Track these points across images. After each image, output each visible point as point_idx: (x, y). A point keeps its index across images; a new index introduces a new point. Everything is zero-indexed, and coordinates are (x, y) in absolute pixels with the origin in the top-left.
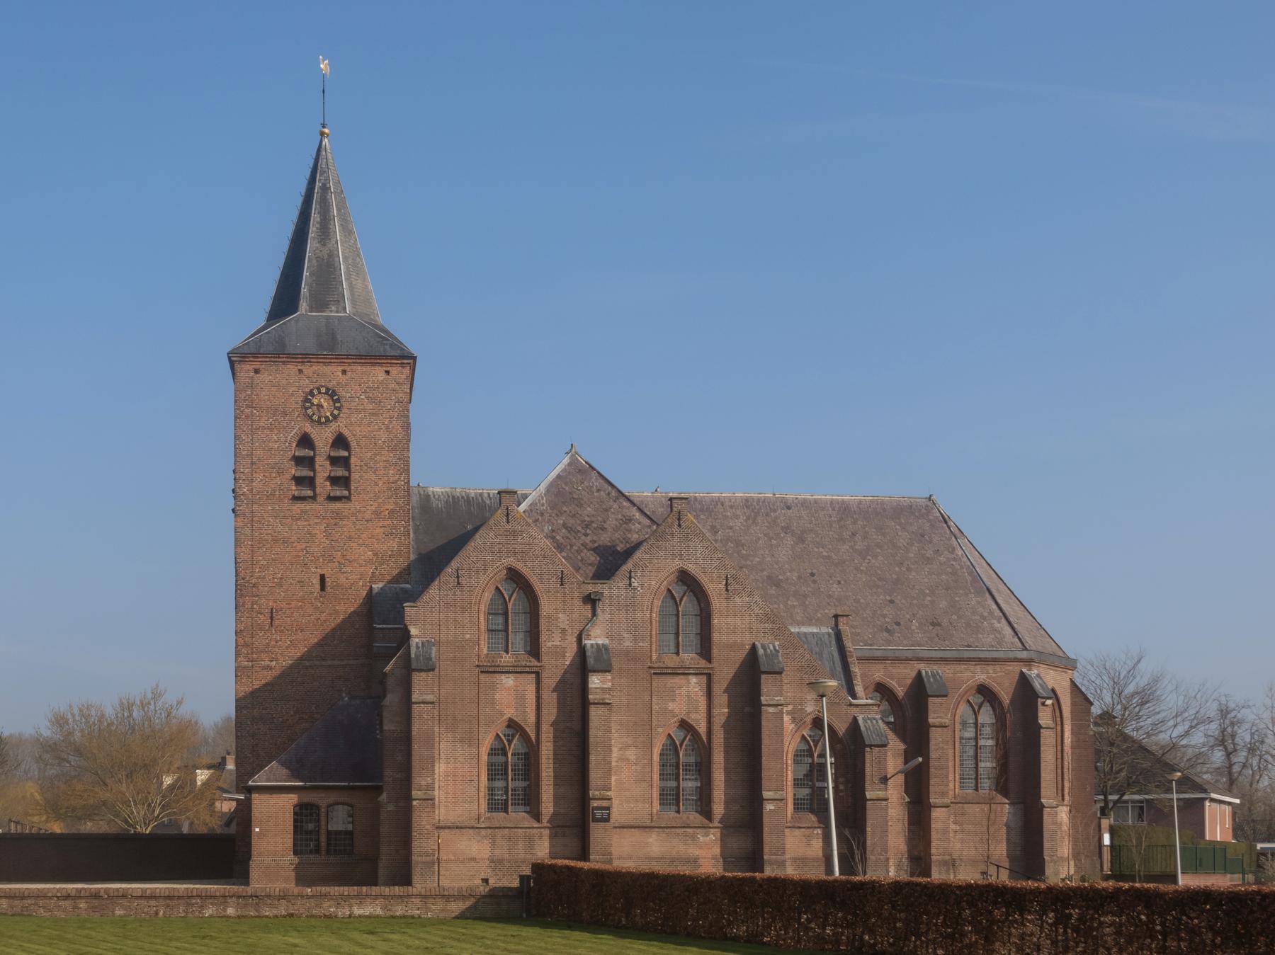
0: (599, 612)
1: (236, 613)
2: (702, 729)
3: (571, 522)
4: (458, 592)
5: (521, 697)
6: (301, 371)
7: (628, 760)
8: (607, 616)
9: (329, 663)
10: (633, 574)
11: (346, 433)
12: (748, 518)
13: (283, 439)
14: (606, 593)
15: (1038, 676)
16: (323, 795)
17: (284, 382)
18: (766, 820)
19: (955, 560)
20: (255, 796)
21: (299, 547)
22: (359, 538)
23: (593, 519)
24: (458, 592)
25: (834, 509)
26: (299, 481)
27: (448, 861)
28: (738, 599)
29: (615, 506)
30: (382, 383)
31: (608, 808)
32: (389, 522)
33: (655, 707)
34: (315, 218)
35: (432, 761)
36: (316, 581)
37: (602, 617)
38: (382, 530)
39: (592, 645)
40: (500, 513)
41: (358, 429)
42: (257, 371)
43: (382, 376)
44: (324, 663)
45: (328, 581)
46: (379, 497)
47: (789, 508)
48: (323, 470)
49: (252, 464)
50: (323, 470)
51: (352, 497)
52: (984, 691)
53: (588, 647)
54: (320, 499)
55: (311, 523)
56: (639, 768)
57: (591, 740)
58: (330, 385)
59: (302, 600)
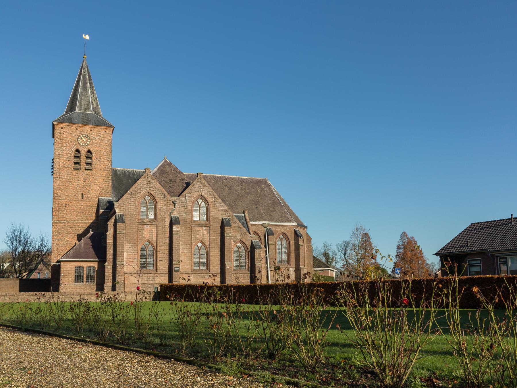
0: (176, 207)
1: (53, 205)
2: (207, 243)
3: (166, 179)
4: (132, 199)
5: (151, 232)
6: (77, 129)
7: (184, 253)
8: (178, 208)
9: (84, 222)
10: (186, 196)
11: (91, 149)
12: (215, 182)
13: (70, 150)
14: (178, 201)
15: (298, 230)
16: (85, 263)
17: (71, 132)
18: (226, 271)
19: (274, 196)
20: (62, 263)
21: (75, 184)
22: (95, 182)
23: (173, 179)
24: (132, 199)
25: (239, 180)
26: (76, 163)
27: (127, 284)
28: (217, 204)
29: (179, 175)
30: (103, 134)
31: (179, 268)
32: (105, 178)
33: (192, 236)
34: (81, 86)
35: (123, 252)
36: (80, 196)
37: (177, 208)
38: (102, 180)
39: (174, 217)
40: (145, 175)
41: (95, 148)
42: (62, 128)
43: (103, 132)
44: (82, 222)
45: (84, 196)
46: (102, 170)
47: (226, 179)
48: (83, 160)
49: (60, 157)
50: (83, 160)
51: (93, 170)
52: (284, 234)
53: (173, 217)
54: (83, 169)
55: (79, 177)
56: (188, 255)
57: (174, 246)
58: (87, 134)
59: (76, 201)
